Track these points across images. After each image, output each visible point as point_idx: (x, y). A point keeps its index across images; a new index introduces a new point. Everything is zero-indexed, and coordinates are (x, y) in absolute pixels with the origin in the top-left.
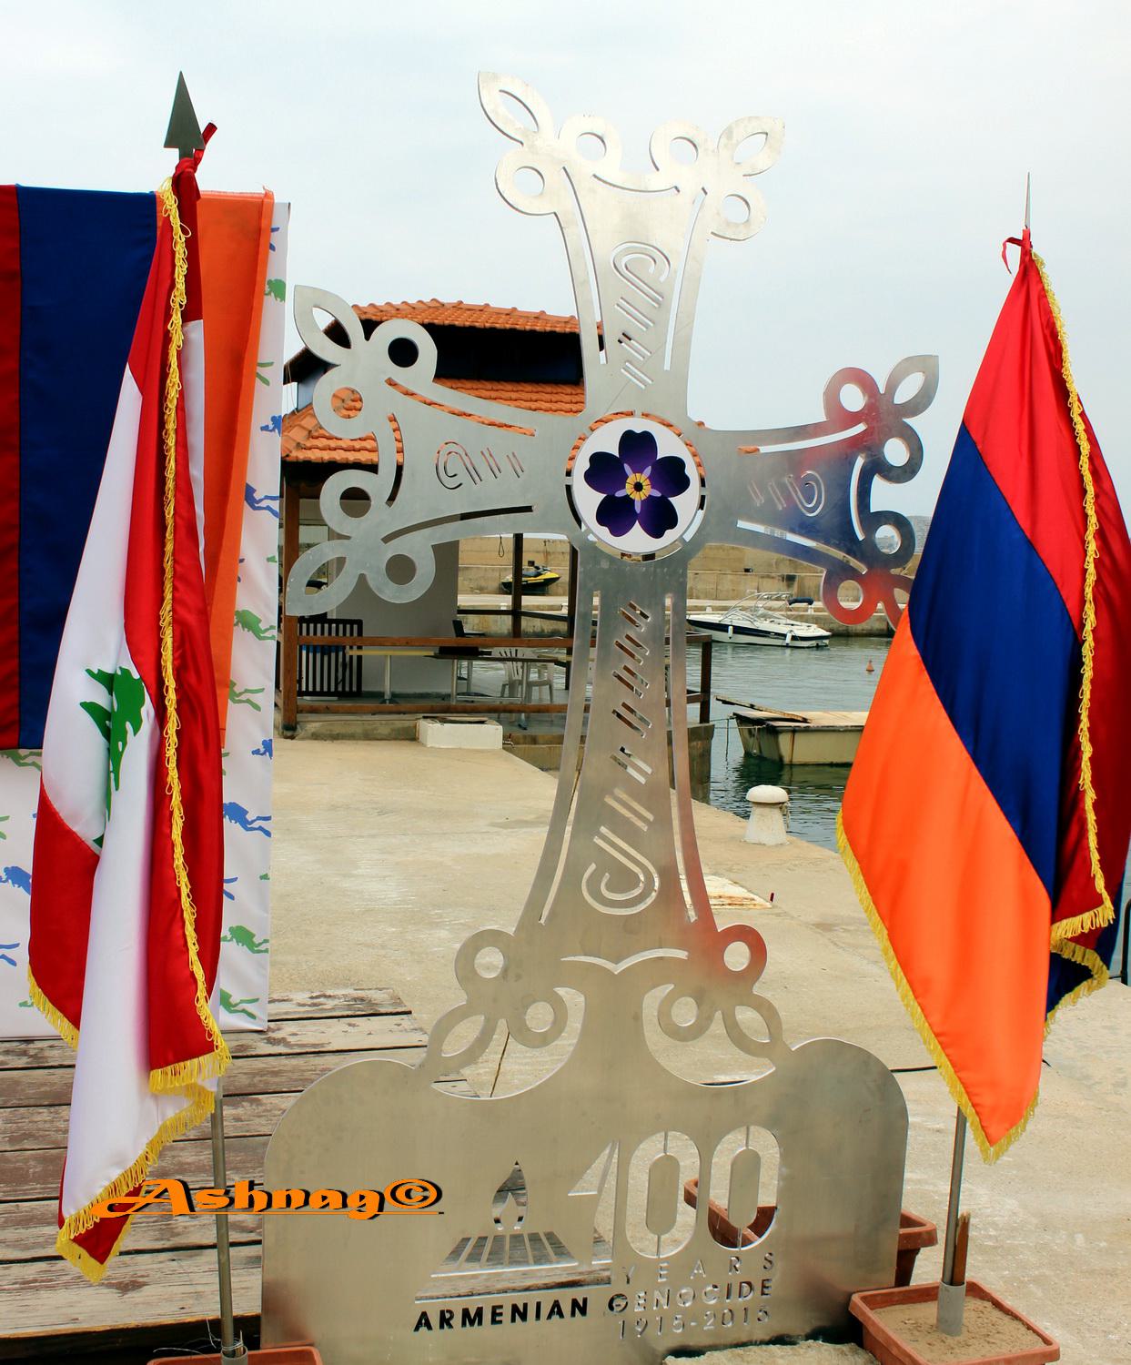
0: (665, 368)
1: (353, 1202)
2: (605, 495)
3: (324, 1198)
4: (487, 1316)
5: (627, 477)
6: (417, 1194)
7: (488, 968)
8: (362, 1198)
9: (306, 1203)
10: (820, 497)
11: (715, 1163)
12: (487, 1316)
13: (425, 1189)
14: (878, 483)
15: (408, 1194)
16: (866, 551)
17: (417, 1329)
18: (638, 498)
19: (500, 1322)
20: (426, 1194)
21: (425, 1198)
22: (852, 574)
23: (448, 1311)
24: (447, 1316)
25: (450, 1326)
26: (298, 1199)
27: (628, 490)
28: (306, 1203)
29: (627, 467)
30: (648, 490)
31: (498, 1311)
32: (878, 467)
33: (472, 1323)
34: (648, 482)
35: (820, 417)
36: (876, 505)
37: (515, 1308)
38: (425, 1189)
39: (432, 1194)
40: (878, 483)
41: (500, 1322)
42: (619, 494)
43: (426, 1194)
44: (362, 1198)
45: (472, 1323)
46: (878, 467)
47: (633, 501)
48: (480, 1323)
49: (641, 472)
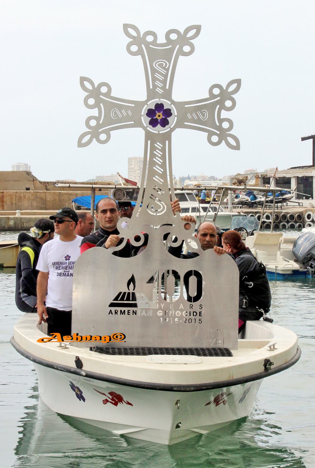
0: (167, 88)
1: (103, 339)
2: (151, 118)
3: (95, 338)
4: (126, 312)
5: (156, 114)
6: (119, 337)
7: (123, 225)
8: (105, 338)
9: (91, 339)
10: (157, 68)
11: (238, 386)
12: (126, 312)
13: (121, 336)
14: (223, 111)
15: (117, 337)
16: (220, 128)
17: (109, 314)
18: (159, 119)
19: (130, 314)
20: (121, 337)
21: (121, 338)
22: (216, 134)
23: (117, 310)
24: (117, 311)
25: (117, 314)
26: (89, 338)
27: (157, 117)
28: (91, 339)
29: (156, 111)
30: (162, 117)
31: (129, 311)
32: (223, 107)
33: (123, 314)
34: (162, 115)
35: (208, 96)
36: (222, 117)
37: (133, 311)
38: (121, 336)
39: (123, 337)
40: (223, 111)
41: (130, 314)
42: (155, 118)
43: (121, 337)
44: (105, 338)
45: (123, 314)
46: (154, 42)
47: (158, 119)
48: (125, 314)
49: (160, 112)
